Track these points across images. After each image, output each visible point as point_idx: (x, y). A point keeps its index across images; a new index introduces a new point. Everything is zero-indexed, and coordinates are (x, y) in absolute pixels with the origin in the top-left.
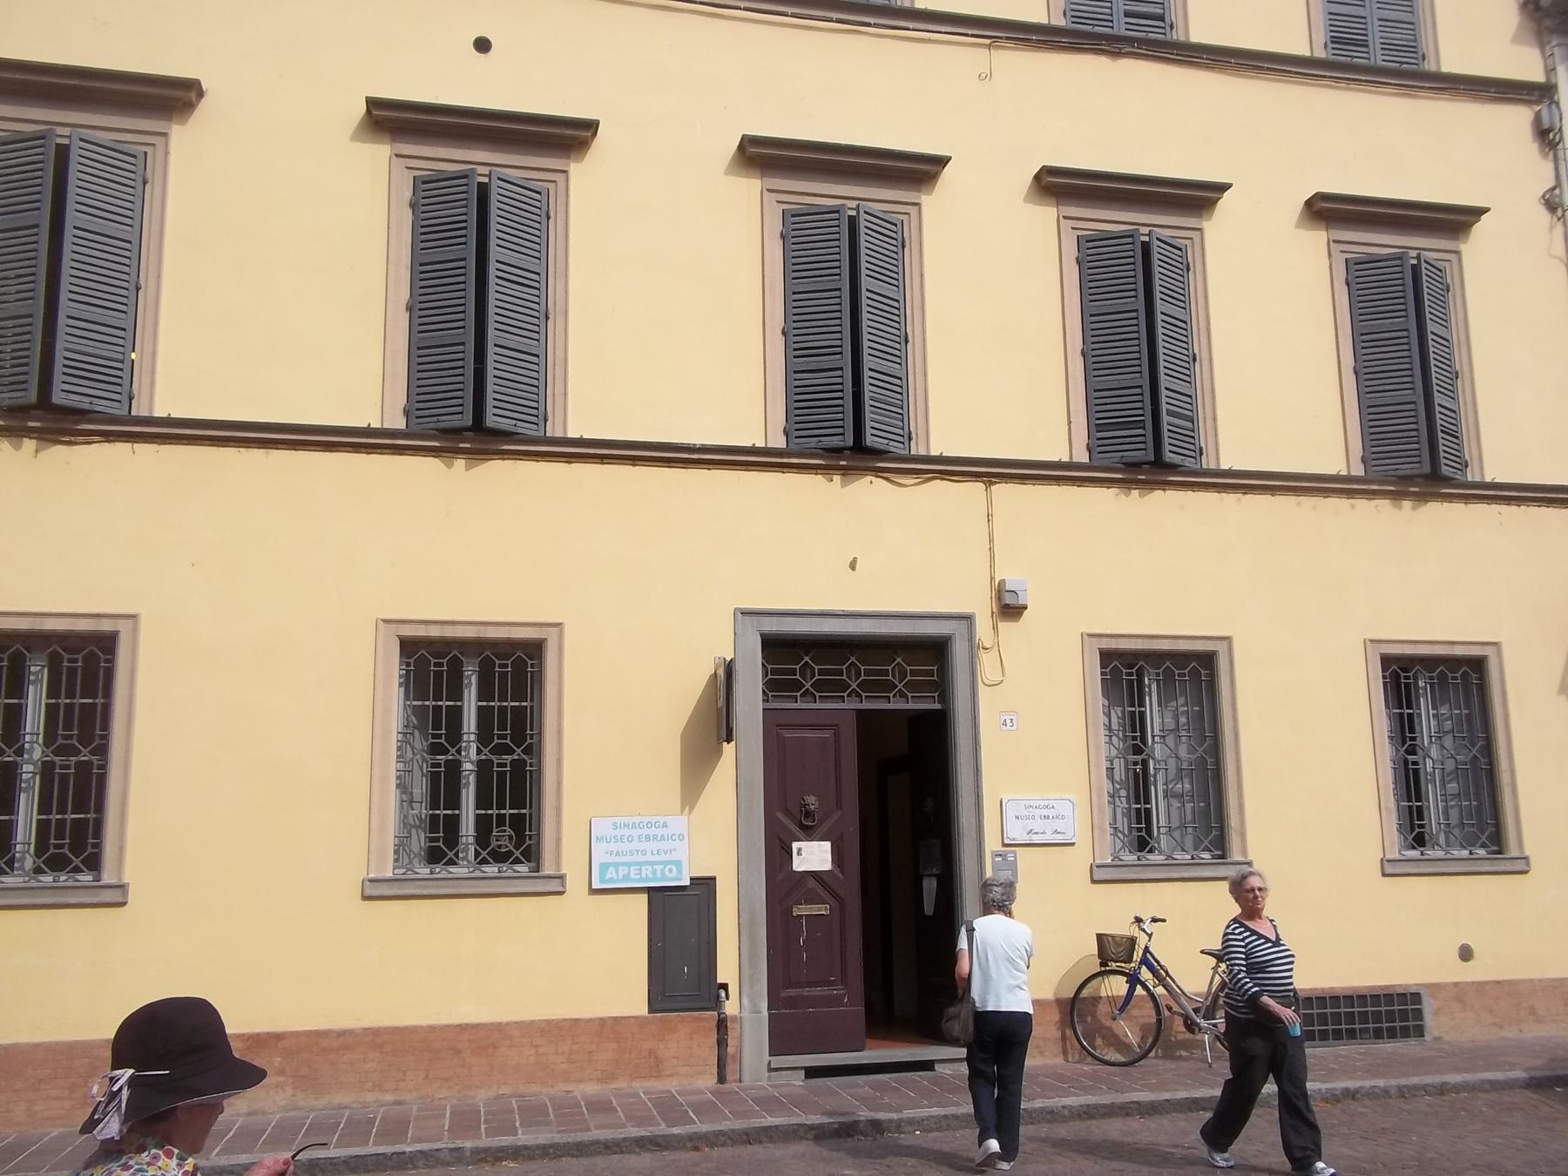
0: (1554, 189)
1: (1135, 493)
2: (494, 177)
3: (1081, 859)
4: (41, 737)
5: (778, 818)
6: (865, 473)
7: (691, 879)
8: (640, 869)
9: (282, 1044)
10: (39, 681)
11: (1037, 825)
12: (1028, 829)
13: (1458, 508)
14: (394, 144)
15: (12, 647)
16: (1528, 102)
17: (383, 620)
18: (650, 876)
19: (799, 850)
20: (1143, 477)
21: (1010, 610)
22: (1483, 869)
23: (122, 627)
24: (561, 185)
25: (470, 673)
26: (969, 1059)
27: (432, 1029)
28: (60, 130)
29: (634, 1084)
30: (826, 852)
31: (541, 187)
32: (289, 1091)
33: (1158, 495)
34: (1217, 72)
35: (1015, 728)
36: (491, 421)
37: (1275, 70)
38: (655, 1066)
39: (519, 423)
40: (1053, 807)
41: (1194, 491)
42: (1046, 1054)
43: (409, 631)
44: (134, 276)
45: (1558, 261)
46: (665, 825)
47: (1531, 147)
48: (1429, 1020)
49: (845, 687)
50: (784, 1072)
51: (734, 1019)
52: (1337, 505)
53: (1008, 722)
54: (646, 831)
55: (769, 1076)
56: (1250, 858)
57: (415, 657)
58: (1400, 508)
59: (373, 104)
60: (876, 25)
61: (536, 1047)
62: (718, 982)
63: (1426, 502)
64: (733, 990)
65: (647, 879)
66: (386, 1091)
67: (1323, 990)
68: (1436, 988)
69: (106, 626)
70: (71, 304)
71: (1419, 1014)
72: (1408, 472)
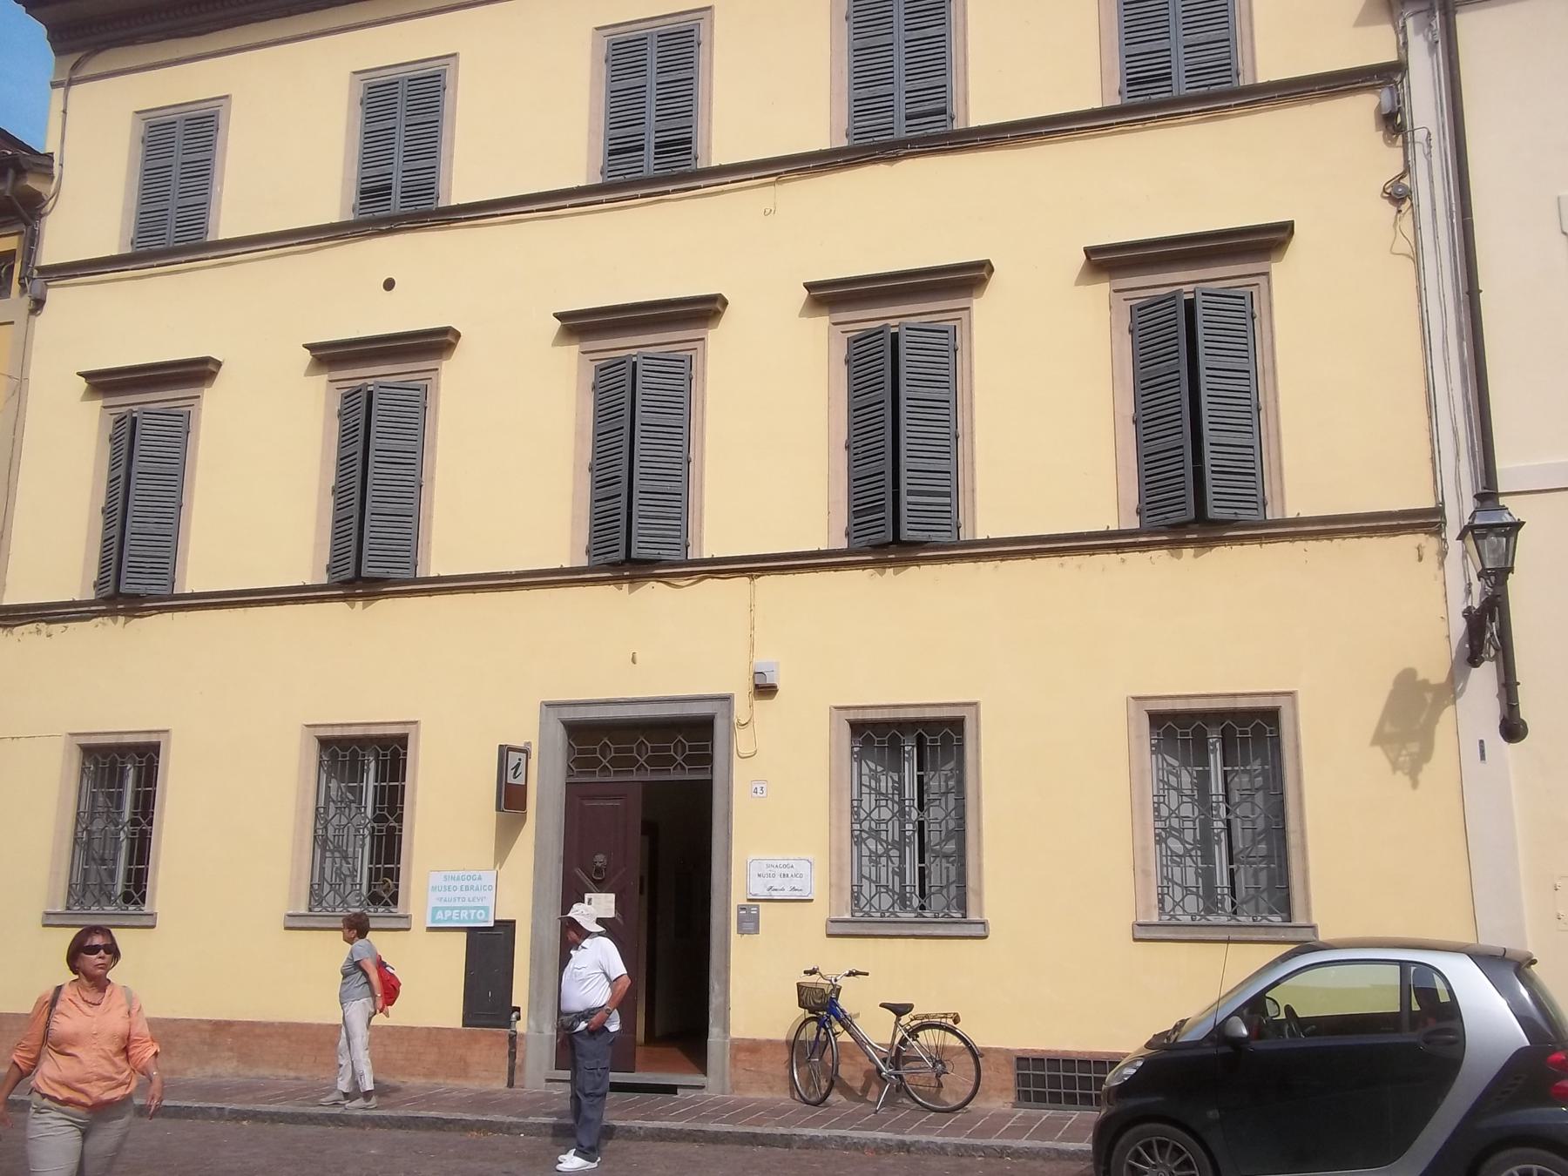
0: (1402, 176)
1: (890, 571)
2: (1199, 293)
3: (819, 913)
4: (916, 801)
5: (575, 873)
6: (376, 598)
7: (496, 921)
8: (460, 913)
9: (233, 1029)
10: (1214, 751)
11: (777, 882)
12: (768, 886)
13: (1251, 549)
14: (1112, 281)
15: (1194, 723)
16: (1372, 88)
17: (836, 708)
18: (466, 918)
19: (590, 900)
20: (893, 556)
21: (765, 690)
22: (1255, 937)
23: (161, 738)
24: (965, 320)
25: (1214, 740)
26: (573, 1081)
27: (320, 1026)
28: (1186, 288)
29: (448, 1081)
30: (611, 902)
31: (1243, 292)
32: (235, 1063)
33: (913, 570)
34: (999, 149)
35: (764, 794)
36: (1213, 512)
38: (464, 1070)
39: (661, 552)
40: (792, 867)
41: (949, 564)
42: (775, 1089)
43: (84, 741)
44: (686, 451)
45: (1404, 257)
46: (480, 878)
49: (672, 760)
50: (557, 1084)
51: (522, 1036)
52: (1108, 561)
53: (759, 790)
54: (465, 883)
55: (546, 1086)
57: (1252, 726)
58: (1179, 557)
59: (1090, 252)
60: (675, 191)
61: (385, 1046)
62: (513, 1005)
63: (1212, 547)
64: (523, 1013)
65: (464, 921)
66: (291, 1069)
69: (153, 738)
70: (642, 482)
72: (1174, 521)
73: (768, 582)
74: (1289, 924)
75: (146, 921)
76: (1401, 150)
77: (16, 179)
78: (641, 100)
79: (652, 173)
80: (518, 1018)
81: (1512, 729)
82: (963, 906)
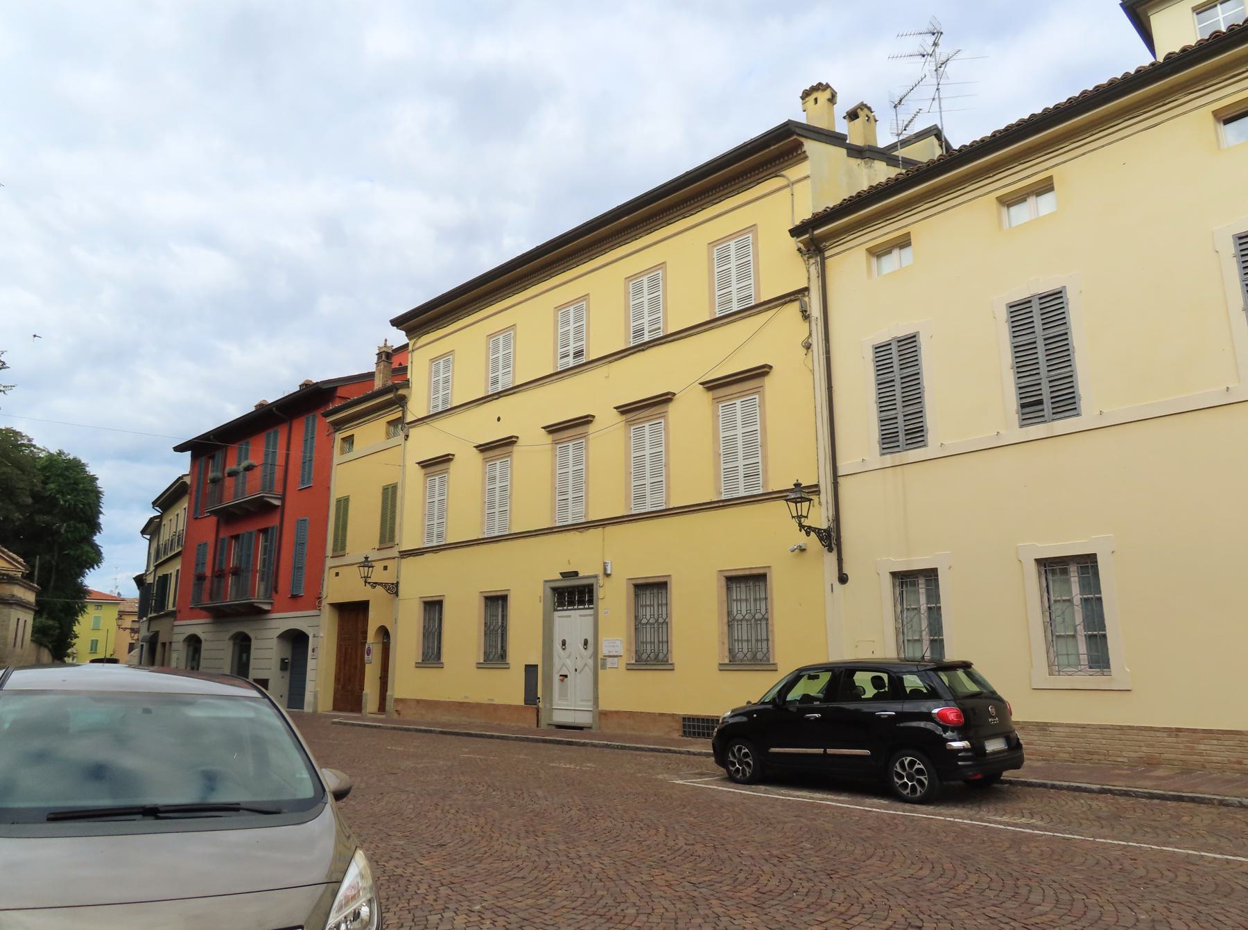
11: (611, 649)
73: (609, 529)
78: (880, 363)
81: (843, 579)
82: (439, 658)
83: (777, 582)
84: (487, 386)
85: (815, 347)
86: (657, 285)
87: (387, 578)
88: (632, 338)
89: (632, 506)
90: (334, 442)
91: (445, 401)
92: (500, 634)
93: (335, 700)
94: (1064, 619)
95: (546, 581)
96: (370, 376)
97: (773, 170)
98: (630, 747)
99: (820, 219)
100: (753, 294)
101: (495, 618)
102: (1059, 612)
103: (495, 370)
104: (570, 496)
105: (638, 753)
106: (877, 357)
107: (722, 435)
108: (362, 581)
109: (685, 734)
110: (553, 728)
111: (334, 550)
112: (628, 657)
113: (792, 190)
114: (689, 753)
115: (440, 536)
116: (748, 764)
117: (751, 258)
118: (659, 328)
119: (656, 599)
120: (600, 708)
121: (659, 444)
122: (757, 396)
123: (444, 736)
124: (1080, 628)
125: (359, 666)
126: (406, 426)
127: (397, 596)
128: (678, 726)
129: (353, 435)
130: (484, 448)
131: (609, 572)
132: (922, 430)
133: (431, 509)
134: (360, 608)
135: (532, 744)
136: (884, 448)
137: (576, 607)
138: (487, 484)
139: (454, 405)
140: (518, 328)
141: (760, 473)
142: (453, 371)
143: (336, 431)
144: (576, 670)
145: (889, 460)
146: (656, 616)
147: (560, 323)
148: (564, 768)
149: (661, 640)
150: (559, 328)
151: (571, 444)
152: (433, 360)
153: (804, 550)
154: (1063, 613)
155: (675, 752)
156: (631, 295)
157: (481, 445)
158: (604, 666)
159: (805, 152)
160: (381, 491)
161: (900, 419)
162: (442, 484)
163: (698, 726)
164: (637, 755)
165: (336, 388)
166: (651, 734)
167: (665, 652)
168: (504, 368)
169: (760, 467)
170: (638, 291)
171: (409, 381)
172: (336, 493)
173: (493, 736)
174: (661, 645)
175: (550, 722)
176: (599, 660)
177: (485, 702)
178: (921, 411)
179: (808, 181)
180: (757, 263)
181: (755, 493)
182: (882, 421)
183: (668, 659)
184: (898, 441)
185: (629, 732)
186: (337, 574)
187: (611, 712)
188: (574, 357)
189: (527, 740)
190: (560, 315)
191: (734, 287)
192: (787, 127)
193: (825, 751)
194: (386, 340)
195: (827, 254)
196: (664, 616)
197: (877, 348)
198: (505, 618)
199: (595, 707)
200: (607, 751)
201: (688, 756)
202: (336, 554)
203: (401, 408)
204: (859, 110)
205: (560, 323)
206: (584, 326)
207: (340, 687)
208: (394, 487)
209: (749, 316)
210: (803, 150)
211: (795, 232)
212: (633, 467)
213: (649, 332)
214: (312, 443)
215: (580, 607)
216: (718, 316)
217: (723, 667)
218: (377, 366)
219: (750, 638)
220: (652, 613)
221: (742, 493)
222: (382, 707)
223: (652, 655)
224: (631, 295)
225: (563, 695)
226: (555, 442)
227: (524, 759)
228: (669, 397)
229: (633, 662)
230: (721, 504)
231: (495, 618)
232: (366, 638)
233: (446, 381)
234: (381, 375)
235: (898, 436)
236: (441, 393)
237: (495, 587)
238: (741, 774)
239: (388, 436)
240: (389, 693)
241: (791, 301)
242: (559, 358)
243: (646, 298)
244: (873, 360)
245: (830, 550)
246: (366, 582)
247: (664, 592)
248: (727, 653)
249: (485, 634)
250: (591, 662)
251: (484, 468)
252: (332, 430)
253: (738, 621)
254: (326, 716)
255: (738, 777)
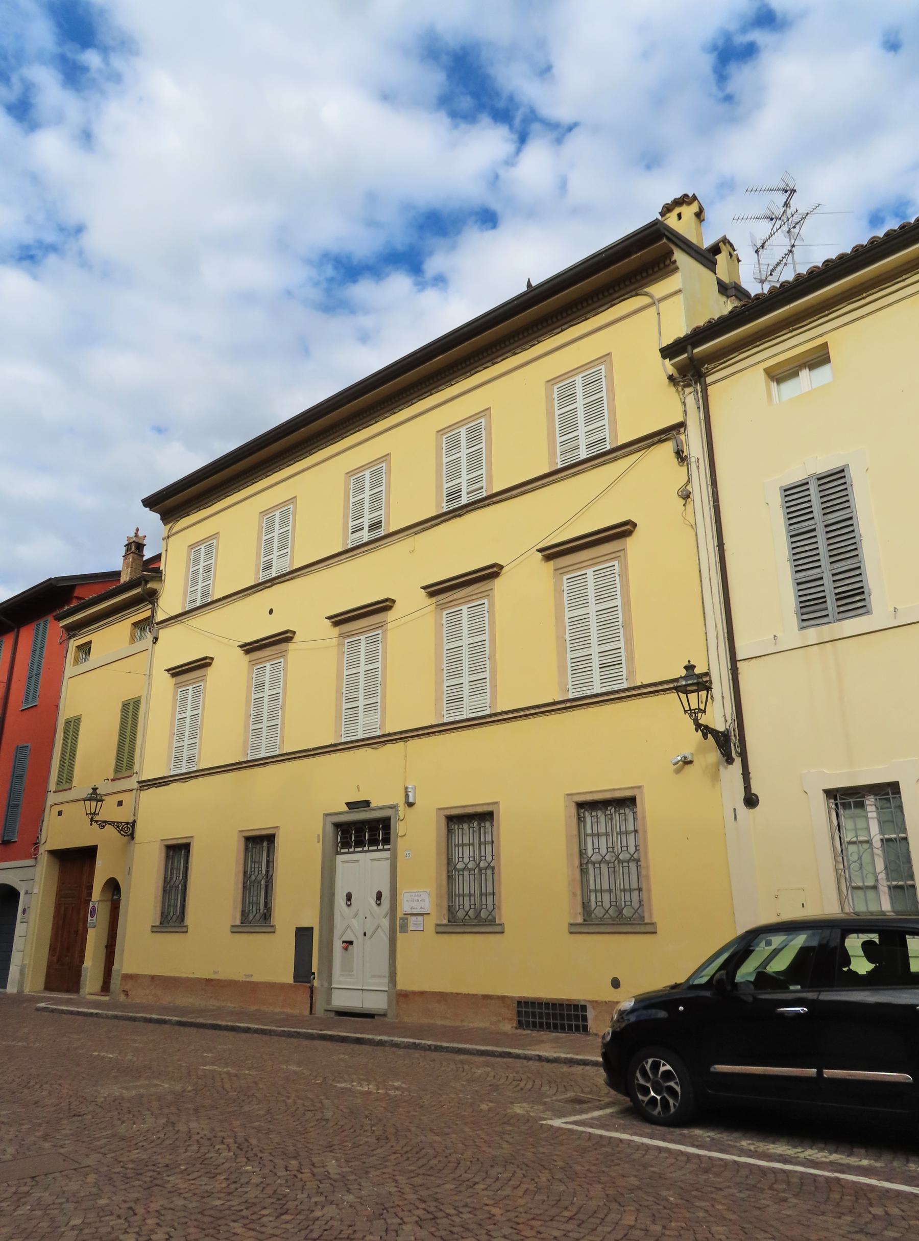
11: (414, 904)
37: (372, 549)
43: (448, 813)
47: (674, 460)
48: (590, 1023)
51: (316, 987)
56: (654, 920)
67: (528, 998)
68: (595, 1003)
71: (585, 1018)
73: (413, 743)
74: (643, 922)
75: (184, 929)
76: (686, 468)
77: (146, 585)
79: (585, 457)
80: (314, 978)
81: (751, 801)
82: (183, 920)
83: (649, 805)
84: (257, 573)
85: (696, 495)
86: (479, 437)
87: (121, 815)
88: (445, 501)
89: (445, 713)
90: (67, 652)
91: (205, 594)
92: (263, 886)
93: (48, 976)
94: (861, 865)
95: (326, 815)
96: (117, 574)
97: (632, 287)
98: (448, 1047)
99: (699, 335)
100: (608, 437)
101: (257, 866)
102: (855, 857)
103: (269, 552)
104: (361, 703)
105: (462, 1057)
106: (786, 502)
107: (568, 615)
108: (88, 819)
109: (520, 1025)
110: (332, 1015)
111: (59, 783)
112: (437, 916)
113: (658, 309)
114: (540, 1058)
115: (191, 760)
116: (672, 1091)
117: (604, 394)
118: (482, 488)
119: (476, 835)
120: (398, 988)
121: (482, 631)
122: (616, 563)
123: (182, 1028)
124: (882, 876)
125: (80, 932)
126: (156, 626)
127: (133, 838)
128: (512, 1013)
129: (90, 642)
130: (250, 648)
131: (411, 800)
132: (863, 593)
133: (182, 726)
134: (88, 855)
135: (305, 1043)
136: (803, 620)
137: (366, 848)
138: (253, 692)
139: (216, 598)
140: (299, 501)
141: (623, 662)
142: (216, 557)
143: (70, 638)
144: (365, 934)
145: (812, 634)
146: (477, 858)
147: (351, 491)
148: (361, 1093)
149: (484, 891)
150: (351, 497)
151: (363, 637)
152: (191, 547)
153: (691, 762)
154: (860, 858)
155: (518, 1057)
156: (444, 450)
157: (247, 644)
158: (404, 928)
159: (675, 261)
160: (120, 706)
161: (828, 580)
162: (196, 696)
163: (548, 1015)
164: (462, 1062)
165: (72, 588)
166: (471, 1025)
167: (490, 907)
168: (279, 549)
169: (623, 654)
170: (454, 445)
171: (162, 573)
172: (66, 712)
173: (249, 1029)
174: (484, 898)
175: (329, 1007)
176: (398, 919)
177: (241, 979)
178: (859, 567)
179: (681, 297)
180: (612, 400)
181: (616, 688)
182: (798, 584)
183: (495, 918)
184: (826, 609)
185: (439, 1022)
186: (60, 813)
187: (414, 993)
188: (370, 531)
189: (298, 1035)
190: (352, 481)
191: (582, 430)
192: (654, 228)
193: (820, 1073)
194: (137, 530)
195: (709, 380)
196: (489, 859)
197: (788, 491)
198: (271, 865)
199: (391, 985)
200: (417, 1054)
201: (537, 1063)
202: (61, 788)
203: (150, 606)
204: (721, 245)
205: (351, 491)
206: (383, 492)
207: (55, 958)
208: (137, 702)
209: (603, 464)
210: (673, 259)
211: (668, 352)
212: (445, 662)
213: (468, 493)
214: (41, 653)
215: (371, 848)
216: (559, 466)
217: (574, 929)
218: (124, 560)
219: (613, 887)
220: (472, 855)
221: (597, 690)
222: (106, 987)
223: (471, 913)
224: (444, 450)
225: (347, 969)
226: (342, 636)
227: (295, 1073)
228: (495, 569)
229: (445, 922)
230: (568, 705)
231: (257, 866)
232: (90, 895)
233: (208, 570)
234: (129, 569)
235: (826, 602)
236: (200, 585)
237: (259, 824)
238: (659, 1108)
239: (133, 639)
240: (116, 967)
241: (661, 441)
242: (350, 533)
243: (464, 452)
244: (782, 507)
245: (729, 760)
246: (92, 820)
247: (488, 824)
248: (579, 909)
249: (244, 887)
250: (386, 923)
251: (250, 672)
252: (65, 636)
253: (594, 863)
254: (33, 999)
255: (656, 1113)
